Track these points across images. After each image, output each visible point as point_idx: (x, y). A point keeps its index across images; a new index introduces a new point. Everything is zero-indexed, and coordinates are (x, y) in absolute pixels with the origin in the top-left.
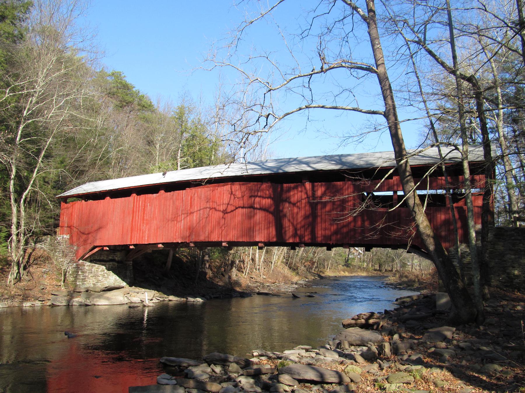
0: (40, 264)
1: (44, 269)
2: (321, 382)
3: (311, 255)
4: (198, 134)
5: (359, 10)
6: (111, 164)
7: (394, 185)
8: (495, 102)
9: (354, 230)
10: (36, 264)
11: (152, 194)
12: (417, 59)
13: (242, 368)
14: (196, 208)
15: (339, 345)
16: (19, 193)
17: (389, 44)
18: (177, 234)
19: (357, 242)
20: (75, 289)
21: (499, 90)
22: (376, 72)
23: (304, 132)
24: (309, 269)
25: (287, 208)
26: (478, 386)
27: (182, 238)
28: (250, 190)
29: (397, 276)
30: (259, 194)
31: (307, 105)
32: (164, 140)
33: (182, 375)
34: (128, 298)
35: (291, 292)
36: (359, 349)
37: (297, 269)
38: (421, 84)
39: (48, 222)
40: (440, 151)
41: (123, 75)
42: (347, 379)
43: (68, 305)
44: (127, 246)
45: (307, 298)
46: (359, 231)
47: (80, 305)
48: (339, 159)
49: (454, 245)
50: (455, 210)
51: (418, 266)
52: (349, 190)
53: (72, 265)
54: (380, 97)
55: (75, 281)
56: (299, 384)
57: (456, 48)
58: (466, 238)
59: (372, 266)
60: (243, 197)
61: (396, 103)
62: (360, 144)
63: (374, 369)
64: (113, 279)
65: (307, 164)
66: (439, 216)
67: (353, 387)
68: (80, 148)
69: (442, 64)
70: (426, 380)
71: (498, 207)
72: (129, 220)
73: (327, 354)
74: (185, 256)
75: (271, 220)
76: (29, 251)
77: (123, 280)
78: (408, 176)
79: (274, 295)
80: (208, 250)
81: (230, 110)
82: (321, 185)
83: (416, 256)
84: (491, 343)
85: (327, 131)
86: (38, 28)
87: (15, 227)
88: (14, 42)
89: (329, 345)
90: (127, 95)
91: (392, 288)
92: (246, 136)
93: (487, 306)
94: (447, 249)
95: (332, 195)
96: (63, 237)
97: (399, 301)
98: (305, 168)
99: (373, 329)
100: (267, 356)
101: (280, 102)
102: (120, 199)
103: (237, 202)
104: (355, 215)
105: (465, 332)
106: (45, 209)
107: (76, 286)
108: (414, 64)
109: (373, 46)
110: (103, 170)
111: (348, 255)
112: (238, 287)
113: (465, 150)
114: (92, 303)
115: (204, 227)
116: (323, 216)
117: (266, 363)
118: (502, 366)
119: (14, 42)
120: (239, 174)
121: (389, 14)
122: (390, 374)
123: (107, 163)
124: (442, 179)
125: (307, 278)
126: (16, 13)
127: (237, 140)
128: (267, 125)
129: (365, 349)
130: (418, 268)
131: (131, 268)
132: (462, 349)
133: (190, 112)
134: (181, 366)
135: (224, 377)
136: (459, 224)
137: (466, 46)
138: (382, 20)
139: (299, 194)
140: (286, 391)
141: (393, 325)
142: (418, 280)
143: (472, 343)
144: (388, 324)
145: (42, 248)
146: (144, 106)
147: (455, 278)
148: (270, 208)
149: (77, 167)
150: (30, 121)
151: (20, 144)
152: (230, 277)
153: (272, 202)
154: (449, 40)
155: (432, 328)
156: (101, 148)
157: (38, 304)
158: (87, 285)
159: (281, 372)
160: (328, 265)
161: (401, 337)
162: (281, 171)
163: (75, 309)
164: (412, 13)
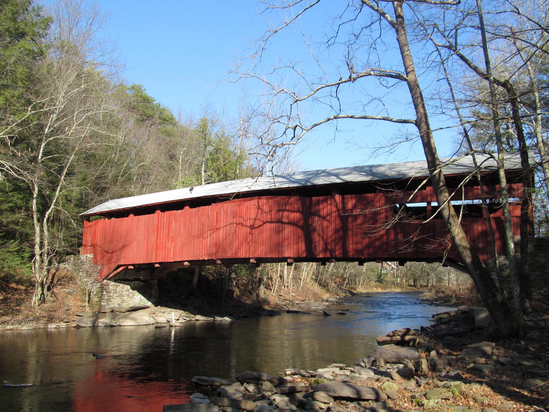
0: (64, 285)
1: (68, 290)
2: (358, 399)
3: (342, 271)
4: (222, 147)
5: (386, 15)
6: (133, 180)
7: (427, 196)
8: (532, 106)
9: (387, 243)
10: (60, 285)
11: (177, 210)
12: (449, 64)
13: (275, 386)
14: (222, 223)
15: (374, 363)
16: (42, 212)
17: (419, 51)
18: (203, 251)
19: (390, 256)
20: (100, 310)
21: (537, 94)
22: (406, 80)
23: (333, 143)
24: (340, 286)
25: (316, 222)
26: (519, 401)
27: (209, 255)
28: (278, 203)
29: (433, 291)
30: (287, 208)
31: (335, 115)
32: (186, 153)
33: (214, 394)
34: (154, 318)
35: (322, 310)
36: (395, 367)
37: (327, 286)
38: (454, 91)
39: (71, 242)
40: (474, 159)
41: (143, 88)
42: (384, 396)
43: (94, 326)
44: (152, 265)
45: (340, 315)
46: (392, 244)
47: (106, 326)
48: (369, 170)
49: (492, 258)
50: (492, 220)
51: (455, 280)
52: (381, 202)
53: (96, 285)
54: (410, 105)
55: (100, 301)
56: (335, 401)
57: (489, 51)
58: (504, 250)
59: (406, 281)
60: (270, 211)
61: (427, 112)
62: (391, 155)
63: (412, 386)
64: (138, 299)
65: (337, 175)
66: (475, 227)
67: (390, 404)
68: (101, 165)
69: (475, 69)
70: (465, 395)
71: (538, 216)
72: (153, 238)
73: (362, 372)
74: (211, 274)
75: (300, 235)
76: (53, 271)
77: (149, 300)
78: (442, 186)
79: (304, 313)
80: (235, 267)
81: (255, 122)
82: (352, 198)
83: (452, 269)
84: (532, 358)
85: (358, 141)
86: (57, 43)
87: (38, 247)
88: (34, 58)
89: (364, 362)
90: (148, 109)
91: (428, 304)
92: (274, 148)
93: (528, 321)
94: (485, 262)
95: (363, 207)
96: (86, 256)
97: (436, 317)
98: (335, 180)
99: (409, 346)
100: (301, 375)
101: (308, 113)
102: (144, 216)
103: (265, 217)
104: (388, 227)
105: (505, 348)
106: (68, 228)
107: (101, 306)
108: (445, 70)
109: (402, 53)
110: (126, 186)
111: (381, 271)
112: (267, 305)
113: (501, 158)
114: (118, 323)
115: (231, 244)
116: (354, 230)
117: (300, 382)
118: (544, 381)
119: (34, 58)
120: (266, 187)
121: (418, 19)
122: (427, 390)
123: (129, 179)
124: (477, 189)
125: (338, 295)
126: (36, 29)
127: (266, 154)
128: (294, 137)
129: (401, 366)
130: (455, 283)
131: (157, 287)
132: (502, 364)
133: (213, 124)
134: (213, 386)
135: (258, 395)
136: (497, 235)
137: (499, 50)
138: (411, 24)
139: (329, 207)
140: (321, 409)
141: (430, 342)
142: (456, 295)
143: (512, 358)
144: (425, 340)
145: (65, 268)
146: (165, 120)
147: (493, 291)
148: (299, 222)
149: (99, 184)
150: (51, 139)
151: (42, 162)
152: (258, 295)
153: (301, 216)
154: (482, 45)
155: (470, 344)
156: (123, 164)
157: (63, 325)
158: (112, 306)
159: (316, 390)
160: (360, 281)
161: (438, 353)
162: (309, 184)
163: (100, 330)
164: (442, 17)
